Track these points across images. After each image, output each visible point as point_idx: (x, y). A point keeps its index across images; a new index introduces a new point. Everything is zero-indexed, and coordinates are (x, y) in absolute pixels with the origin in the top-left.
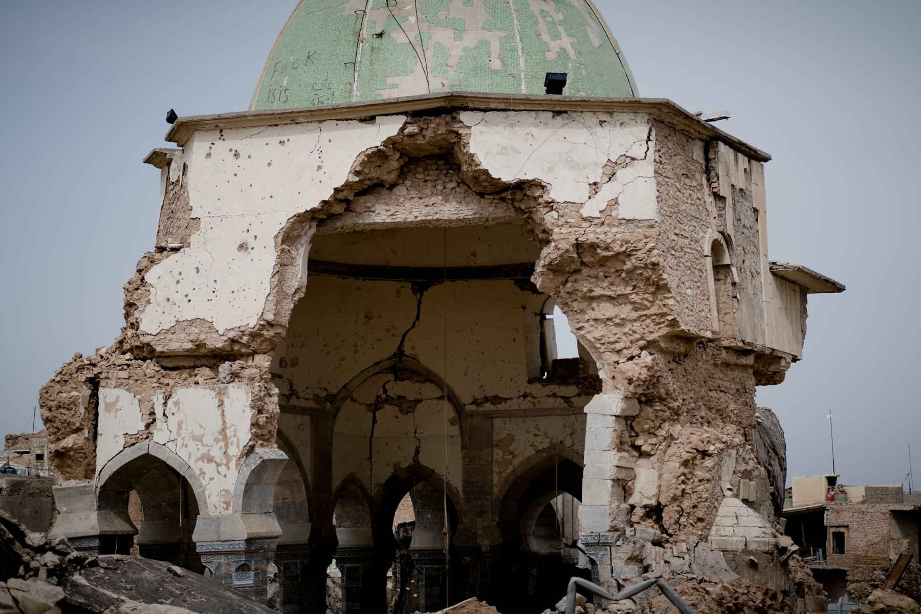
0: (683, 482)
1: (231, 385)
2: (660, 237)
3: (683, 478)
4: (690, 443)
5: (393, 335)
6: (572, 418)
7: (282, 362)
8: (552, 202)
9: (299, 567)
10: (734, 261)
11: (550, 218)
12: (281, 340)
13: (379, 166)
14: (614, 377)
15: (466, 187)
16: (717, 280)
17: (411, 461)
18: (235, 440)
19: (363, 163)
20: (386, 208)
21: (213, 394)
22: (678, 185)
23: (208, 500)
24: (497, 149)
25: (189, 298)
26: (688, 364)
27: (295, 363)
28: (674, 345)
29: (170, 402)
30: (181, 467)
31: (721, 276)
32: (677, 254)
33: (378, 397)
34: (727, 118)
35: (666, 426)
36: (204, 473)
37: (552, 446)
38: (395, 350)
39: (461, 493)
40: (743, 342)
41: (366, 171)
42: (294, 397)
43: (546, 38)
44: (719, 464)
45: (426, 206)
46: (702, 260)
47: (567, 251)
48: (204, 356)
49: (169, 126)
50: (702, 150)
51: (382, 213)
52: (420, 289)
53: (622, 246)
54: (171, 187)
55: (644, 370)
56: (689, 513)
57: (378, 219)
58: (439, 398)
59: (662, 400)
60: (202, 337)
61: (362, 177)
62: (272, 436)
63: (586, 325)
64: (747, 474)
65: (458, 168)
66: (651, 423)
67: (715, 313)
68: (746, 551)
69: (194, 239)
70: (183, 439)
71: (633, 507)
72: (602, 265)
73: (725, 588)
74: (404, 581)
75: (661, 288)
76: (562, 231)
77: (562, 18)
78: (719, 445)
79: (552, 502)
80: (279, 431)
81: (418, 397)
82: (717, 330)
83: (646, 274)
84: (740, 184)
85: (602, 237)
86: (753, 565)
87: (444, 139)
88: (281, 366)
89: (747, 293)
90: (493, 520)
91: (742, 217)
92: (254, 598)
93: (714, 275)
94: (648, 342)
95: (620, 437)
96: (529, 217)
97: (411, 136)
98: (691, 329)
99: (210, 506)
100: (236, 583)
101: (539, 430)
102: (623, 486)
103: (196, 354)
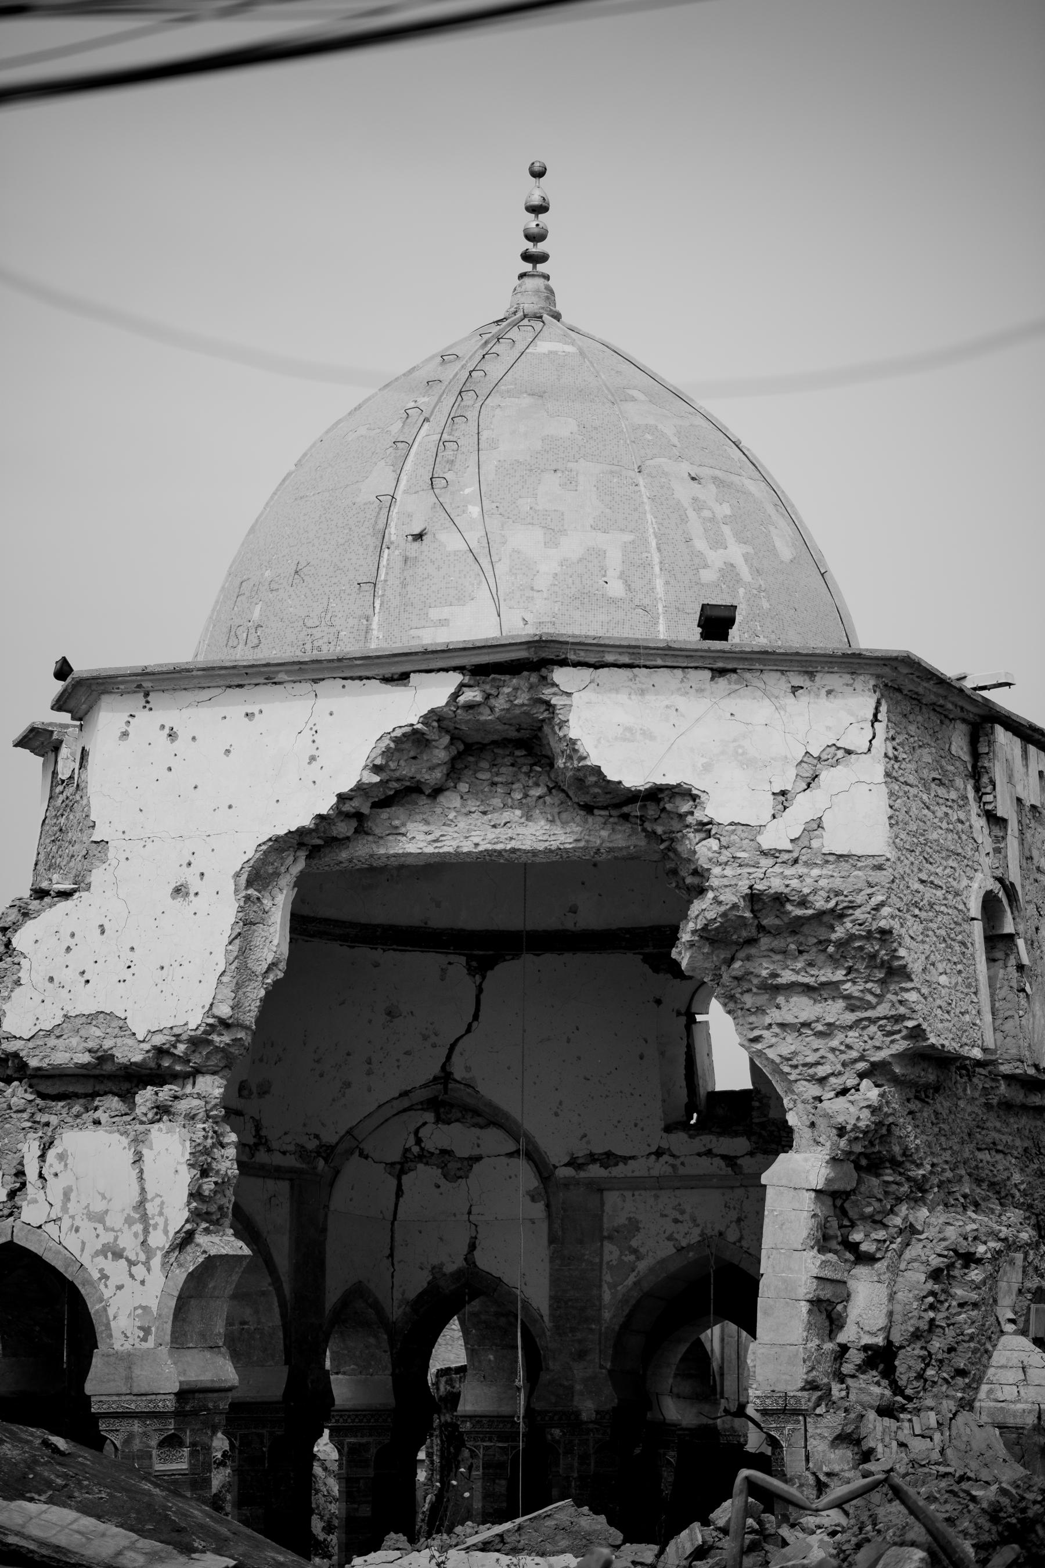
0: (932, 1307)
1: (156, 1126)
2: (894, 886)
3: (931, 1299)
4: (944, 1239)
6: (740, 1192)
8: (710, 823)
10: (1021, 928)
11: (705, 850)
13: (414, 758)
14: (813, 1125)
15: (562, 795)
16: (991, 960)
17: (459, 1263)
18: (160, 1221)
19: (387, 753)
20: (426, 828)
21: (125, 1141)
22: (925, 797)
24: (613, 730)
25: (86, 977)
26: (942, 1104)
27: (264, 1091)
28: (917, 1070)
29: (51, 1154)
30: (67, 1266)
31: (999, 955)
32: (923, 915)
33: (407, 1150)
34: (1009, 684)
35: (903, 1209)
37: (705, 1240)
38: (436, 1070)
39: (546, 1319)
40: (1036, 1066)
41: (392, 765)
44: (992, 1278)
45: (494, 826)
46: (965, 926)
47: (735, 906)
48: (111, 1077)
49: (59, 686)
50: (967, 739)
52: (480, 967)
53: (828, 899)
55: (866, 1114)
56: (941, 1361)
57: (412, 848)
58: (510, 1155)
59: (895, 1164)
60: (107, 1044)
61: (385, 776)
62: (224, 1215)
63: (766, 1033)
66: (877, 1205)
67: (988, 1017)
69: (97, 876)
70: (73, 1217)
72: (794, 932)
73: (1003, 1492)
74: (447, 1467)
75: (895, 973)
76: (726, 872)
77: (728, 512)
78: (992, 1244)
79: (702, 1337)
81: (476, 1152)
82: (992, 1046)
83: (869, 949)
85: (795, 883)
87: (525, 713)
88: (240, 1096)
90: (601, 1367)
91: (1035, 853)
92: (188, 1494)
93: (987, 952)
94: (873, 1064)
96: (669, 849)
97: (470, 707)
98: (946, 1043)
99: (116, 1333)
100: (159, 1467)
101: (683, 1212)
102: (828, 1311)
103: (97, 1072)
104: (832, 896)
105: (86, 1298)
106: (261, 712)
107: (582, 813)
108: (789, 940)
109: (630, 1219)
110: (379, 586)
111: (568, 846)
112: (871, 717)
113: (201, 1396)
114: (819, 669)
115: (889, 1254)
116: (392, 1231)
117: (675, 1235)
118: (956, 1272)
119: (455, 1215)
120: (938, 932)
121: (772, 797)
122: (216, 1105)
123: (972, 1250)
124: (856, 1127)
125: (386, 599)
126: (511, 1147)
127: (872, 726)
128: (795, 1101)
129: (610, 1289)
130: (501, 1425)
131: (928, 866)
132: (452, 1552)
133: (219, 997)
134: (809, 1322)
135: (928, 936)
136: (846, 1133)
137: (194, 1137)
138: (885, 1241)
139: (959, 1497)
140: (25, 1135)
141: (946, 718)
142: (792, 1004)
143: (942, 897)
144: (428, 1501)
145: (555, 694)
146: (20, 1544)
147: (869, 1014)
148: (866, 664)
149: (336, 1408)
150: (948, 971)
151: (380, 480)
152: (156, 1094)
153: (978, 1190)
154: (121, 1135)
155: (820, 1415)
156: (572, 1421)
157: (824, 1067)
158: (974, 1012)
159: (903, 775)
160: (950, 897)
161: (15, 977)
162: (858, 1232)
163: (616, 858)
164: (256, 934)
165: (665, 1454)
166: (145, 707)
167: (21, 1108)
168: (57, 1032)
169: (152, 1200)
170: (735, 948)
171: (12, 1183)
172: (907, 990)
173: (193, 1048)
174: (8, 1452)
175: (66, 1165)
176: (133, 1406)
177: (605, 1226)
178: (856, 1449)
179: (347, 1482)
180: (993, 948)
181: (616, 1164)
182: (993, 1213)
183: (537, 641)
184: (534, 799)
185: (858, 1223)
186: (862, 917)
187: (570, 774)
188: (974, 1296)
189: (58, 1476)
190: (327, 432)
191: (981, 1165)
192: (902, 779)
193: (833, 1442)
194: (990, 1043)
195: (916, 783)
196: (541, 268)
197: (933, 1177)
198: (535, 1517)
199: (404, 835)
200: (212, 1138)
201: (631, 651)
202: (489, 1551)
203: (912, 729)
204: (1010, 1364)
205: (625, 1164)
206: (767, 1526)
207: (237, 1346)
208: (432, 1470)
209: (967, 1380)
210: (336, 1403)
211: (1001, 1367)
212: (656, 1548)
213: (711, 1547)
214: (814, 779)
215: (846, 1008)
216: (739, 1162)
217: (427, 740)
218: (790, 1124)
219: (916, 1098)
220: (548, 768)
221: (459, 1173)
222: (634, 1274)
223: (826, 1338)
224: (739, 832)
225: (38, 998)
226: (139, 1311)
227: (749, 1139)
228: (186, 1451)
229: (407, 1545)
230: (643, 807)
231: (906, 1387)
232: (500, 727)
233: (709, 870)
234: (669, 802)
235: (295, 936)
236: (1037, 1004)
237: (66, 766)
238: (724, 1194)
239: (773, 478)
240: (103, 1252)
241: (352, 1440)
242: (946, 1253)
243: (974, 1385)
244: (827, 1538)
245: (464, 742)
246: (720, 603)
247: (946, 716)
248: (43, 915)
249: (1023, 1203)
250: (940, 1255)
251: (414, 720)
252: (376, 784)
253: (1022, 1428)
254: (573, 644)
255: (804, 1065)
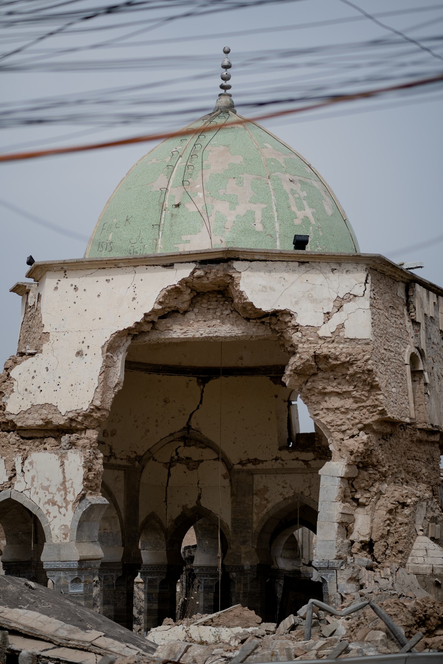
0: (389, 525)
1: (70, 451)
2: (374, 351)
3: (388, 522)
4: (394, 497)
5: (184, 415)
6: (310, 475)
7: (104, 433)
8: (298, 326)
9: (115, 579)
10: (426, 368)
11: (296, 337)
12: (105, 420)
13: (176, 298)
14: (340, 450)
15: (237, 314)
16: (414, 381)
17: (194, 504)
18: (72, 490)
19: (165, 296)
20: (181, 327)
21: (57, 457)
22: (386, 314)
23: (52, 532)
24: (258, 288)
25: (41, 389)
26: (393, 441)
27: (113, 434)
28: (383, 427)
29: (26, 462)
30: (33, 508)
31: (417, 379)
32: (386, 363)
33: (172, 458)
34: (421, 267)
35: (377, 485)
36: (50, 513)
37: (295, 495)
38: (185, 425)
39: (230, 527)
40: (432, 425)
41: (167, 302)
42: (112, 457)
43: (294, 209)
44: (414, 513)
45: (209, 327)
46: (403, 367)
47: (308, 360)
48: (51, 430)
49: (29, 267)
50: (404, 289)
51: (178, 331)
52: (203, 382)
53: (346, 357)
54: (29, 310)
55: (362, 446)
56: (392, 547)
57: (175, 336)
58: (215, 460)
59: (374, 466)
60: (50, 417)
61: (164, 306)
62: (98, 487)
63: (321, 412)
64: (434, 520)
65: (232, 300)
66: (366, 483)
67: (412, 405)
68: (433, 575)
69: (45, 347)
70: (35, 488)
71: (353, 542)
72: (332, 371)
73: (417, 604)
74: (189, 586)
75: (374, 387)
76: (304, 346)
77: (306, 195)
78: (414, 499)
79: (294, 533)
80: (103, 484)
81: (201, 458)
82: (414, 417)
83: (363, 377)
84: (431, 313)
85: (333, 350)
86: (437, 584)
87: (221, 280)
88: (104, 436)
89: (435, 390)
90: (253, 547)
91: (432, 336)
92: (83, 603)
93: (412, 378)
94: (365, 425)
95: (344, 492)
96: (281, 336)
97: (199, 277)
98: (395, 416)
99: (54, 536)
100: (71, 591)
101: (286, 483)
102: (346, 527)
103: (45, 428)
104: (348, 356)
105: (41, 521)
106: (112, 279)
107: (245, 321)
108: (330, 374)
109: (264, 486)
110: (161, 226)
111: (239, 335)
112: (364, 281)
113: (89, 562)
114: (343, 261)
115: (371, 503)
116: (166, 491)
117: (283, 493)
118: (399, 510)
119: (192, 484)
120: (392, 370)
121: (323, 315)
122: (94, 442)
123: (405, 501)
124: (357, 451)
125: (164, 232)
126: (216, 456)
127: (365, 285)
128: (333, 440)
129: (256, 515)
130: (211, 570)
131: (388, 343)
132: (192, 626)
133: (95, 397)
134: (338, 531)
135: (387, 372)
136: (354, 453)
137: (86, 455)
138: (369, 498)
139: (399, 605)
140: (16, 454)
141: (395, 281)
142: (331, 400)
143: (393, 356)
144: (181, 601)
145: (234, 272)
146: (16, 626)
147: (363, 404)
148: (363, 259)
149: (143, 564)
150: (396, 386)
151: (161, 182)
152: (70, 437)
153: (408, 476)
154: (55, 454)
155: (343, 570)
156: (241, 570)
157: (345, 426)
158: (406, 403)
159: (377, 305)
160: (397, 355)
161: (11, 389)
162: (359, 494)
163: (259, 340)
164: (111, 371)
165: (279, 582)
166: (64, 277)
167: (14, 443)
168: (29, 412)
169: (68, 481)
170: (308, 377)
171: (11, 474)
172: (379, 395)
173: (85, 418)
174: (11, 588)
175: (33, 467)
176: (60, 566)
177: (254, 489)
178: (357, 583)
179: (148, 595)
180: (414, 376)
181: (259, 464)
182: (414, 486)
183: (226, 251)
184: (225, 315)
185: (358, 490)
186: (360, 364)
187: (240, 305)
188: (406, 520)
189: (32, 598)
190: (139, 161)
191: (409, 466)
192: (377, 307)
193: (348, 581)
194: (413, 416)
195: (383, 308)
196: (228, 91)
197: (389, 471)
198: (226, 611)
199: (171, 330)
200: (93, 455)
201: (265, 254)
202: (207, 625)
203: (381, 286)
204: (421, 548)
205: (263, 463)
206: (321, 616)
207: (103, 540)
208: (182, 588)
209: (403, 555)
210: (143, 562)
211: (417, 549)
212: (275, 624)
213: (298, 625)
214: (341, 307)
215: (354, 402)
216: (310, 463)
217: (181, 291)
218: (330, 449)
219: (382, 438)
220: (231, 303)
221: (194, 467)
222: (266, 509)
223: (345, 538)
224: (310, 330)
225: (21, 398)
226: (63, 527)
227: (314, 453)
228: (82, 585)
229: (173, 623)
230: (270, 319)
231: (378, 558)
232: (211, 286)
233: (297, 345)
234: (281, 317)
235: (126, 370)
236: (433, 399)
237: (31, 301)
238: (303, 476)
239: (324, 180)
240: (48, 502)
241: (150, 577)
242: (394, 502)
243: (406, 557)
244: (345, 621)
245: (196, 292)
246: (302, 234)
247: (395, 280)
248: (23, 363)
249: (427, 481)
250: (392, 504)
251: (176, 283)
252: (160, 309)
253: (426, 575)
254: (241, 251)
255: (336, 425)
